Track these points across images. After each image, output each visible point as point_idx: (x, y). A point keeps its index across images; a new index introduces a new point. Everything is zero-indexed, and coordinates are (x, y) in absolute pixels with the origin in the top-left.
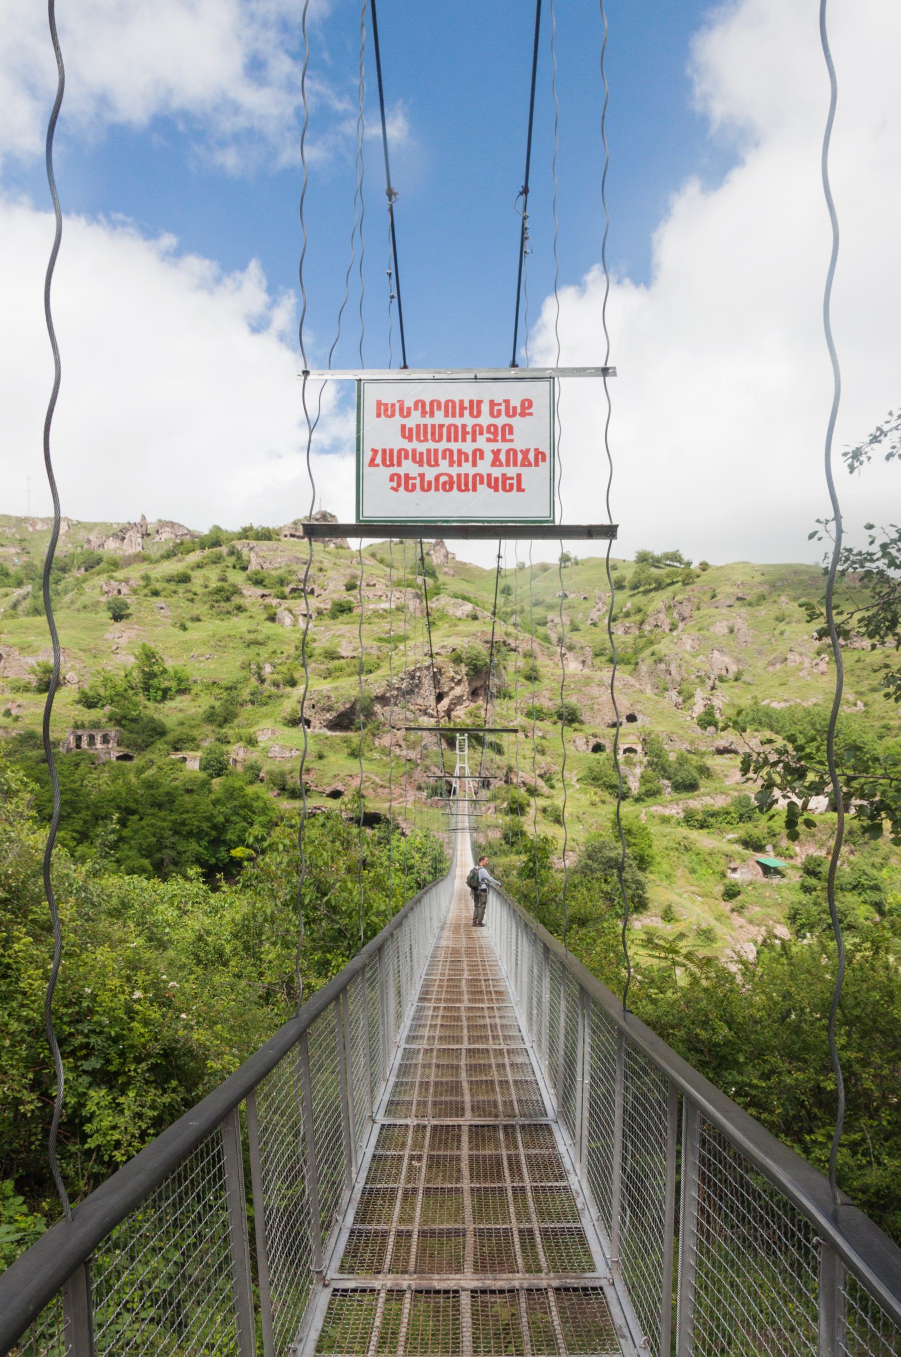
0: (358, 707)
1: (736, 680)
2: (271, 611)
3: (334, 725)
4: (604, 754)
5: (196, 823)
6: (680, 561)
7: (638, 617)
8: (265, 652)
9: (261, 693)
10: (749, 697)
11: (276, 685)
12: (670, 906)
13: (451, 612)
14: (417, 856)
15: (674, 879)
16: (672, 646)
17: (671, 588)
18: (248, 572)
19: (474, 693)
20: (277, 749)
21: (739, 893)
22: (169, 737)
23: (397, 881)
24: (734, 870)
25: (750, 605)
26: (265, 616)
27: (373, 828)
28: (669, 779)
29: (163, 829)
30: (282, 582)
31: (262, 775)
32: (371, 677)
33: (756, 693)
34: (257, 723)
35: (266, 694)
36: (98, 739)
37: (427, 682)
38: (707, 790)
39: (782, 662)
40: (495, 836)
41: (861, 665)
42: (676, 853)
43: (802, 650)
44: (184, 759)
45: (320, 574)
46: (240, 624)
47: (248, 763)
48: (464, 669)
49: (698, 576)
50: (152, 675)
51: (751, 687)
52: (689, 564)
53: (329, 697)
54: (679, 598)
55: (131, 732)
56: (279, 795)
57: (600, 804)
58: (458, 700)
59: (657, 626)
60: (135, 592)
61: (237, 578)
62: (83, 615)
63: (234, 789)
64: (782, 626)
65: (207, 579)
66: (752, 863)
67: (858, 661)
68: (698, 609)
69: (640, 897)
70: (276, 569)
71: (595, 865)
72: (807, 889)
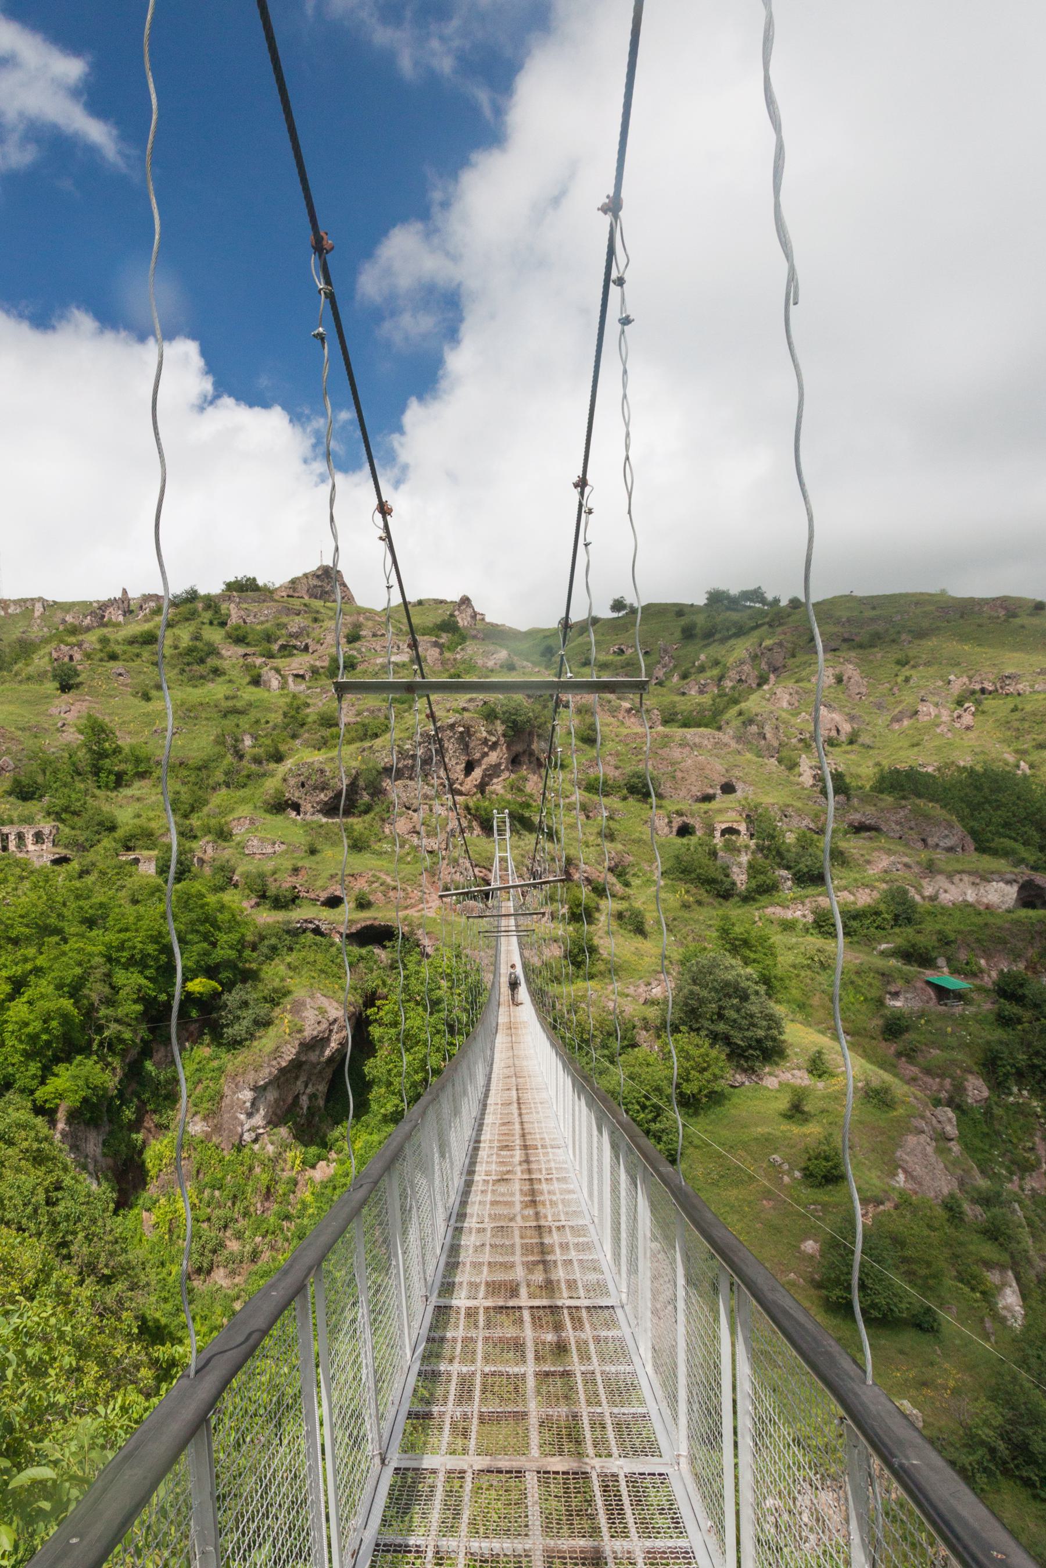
0: (361, 783)
1: (851, 742)
2: (255, 672)
3: (330, 809)
4: (694, 839)
5: (139, 946)
6: (763, 600)
7: (716, 672)
8: (245, 722)
9: (238, 772)
10: (871, 764)
11: (257, 760)
12: (819, 1052)
13: (480, 662)
14: (444, 984)
15: (809, 1010)
16: (764, 703)
17: (756, 633)
18: (227, 628)
19: (515, 761)
20: (255, 842)
21: (907, 1029)
22: (120, 833)
23: (418, 1022)
24: (895, 995)
25: (861, 646)
26: (248, 679)
27: (384, 947)
28: (788, 868)
29: (91, 955)
30: (269, 638)
31: (235, 878)
32: (378, 742)
33: (880, 759)
34: (232, 810)
35: (244, 773)
36: (29, 839)
37: (451, 746)
38: (844, 882)
39: (911, 717)
40: (555, 952)
41: (1018, 715)
42: (809, 973)
43: (936, 699)
44: (136, 861)
45: (315, 625)
46: (217, 690)
47: (218, 863)
48: (500, 728)
49: (789, 616)
50: (103, 755)
51: (871, 752)
52: (777, 601)
53: (322, 771)
54: (768, 643)
55: (73, 828)
56: (258, 905)
57: (695, 906)
58: (494, 771)
59: (740, 681)
60: (88, 656)
61: (215, 636)
62: (24, 687)
63: (190, 896)
64: (906, 671)
65: (177, 638)
66: (919, 984)
67: (1015, 710)
68: (794, 656)
69: (774, 1039)
70: (262, 623)
71: (704, 993)
72: (1004, 1021)
